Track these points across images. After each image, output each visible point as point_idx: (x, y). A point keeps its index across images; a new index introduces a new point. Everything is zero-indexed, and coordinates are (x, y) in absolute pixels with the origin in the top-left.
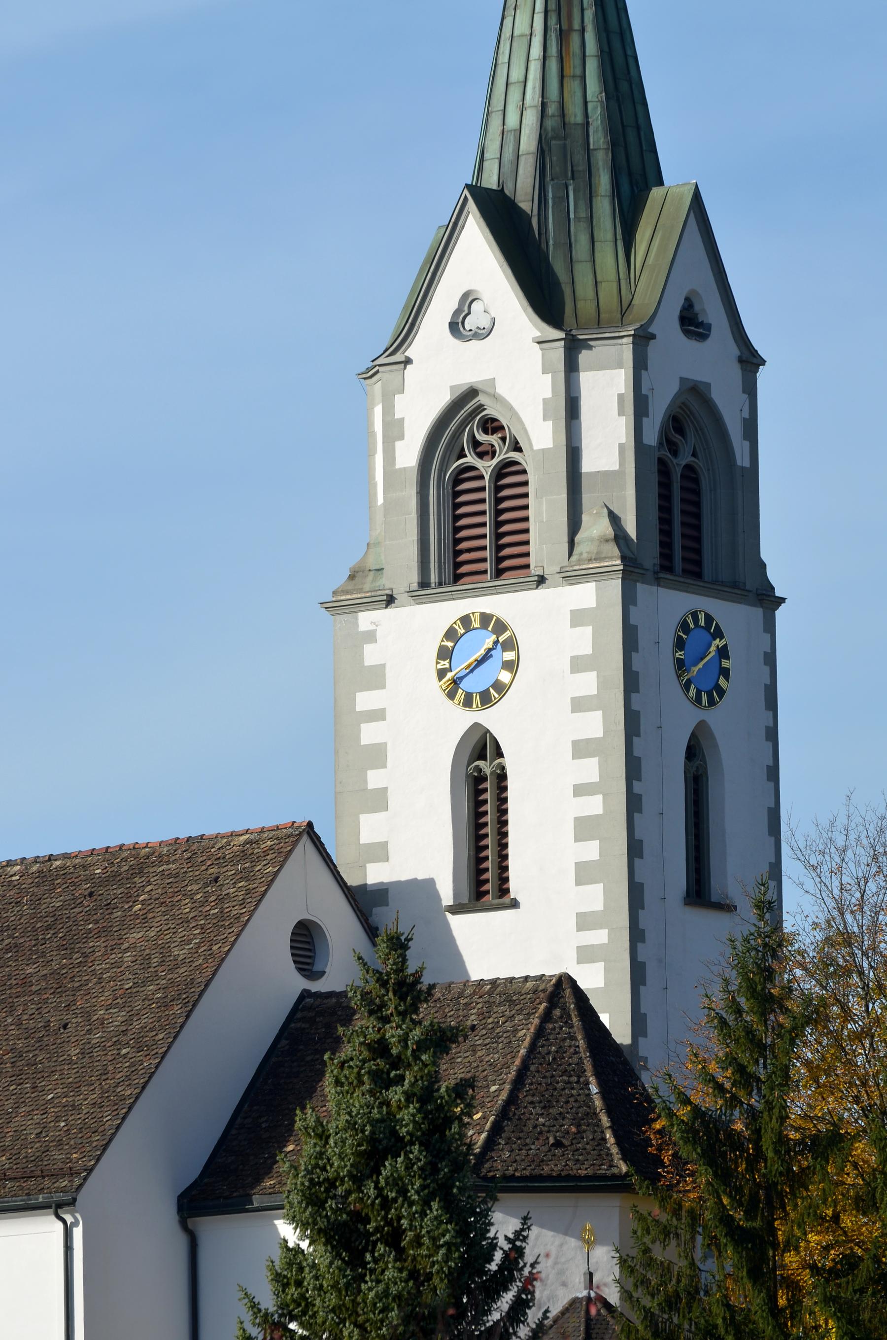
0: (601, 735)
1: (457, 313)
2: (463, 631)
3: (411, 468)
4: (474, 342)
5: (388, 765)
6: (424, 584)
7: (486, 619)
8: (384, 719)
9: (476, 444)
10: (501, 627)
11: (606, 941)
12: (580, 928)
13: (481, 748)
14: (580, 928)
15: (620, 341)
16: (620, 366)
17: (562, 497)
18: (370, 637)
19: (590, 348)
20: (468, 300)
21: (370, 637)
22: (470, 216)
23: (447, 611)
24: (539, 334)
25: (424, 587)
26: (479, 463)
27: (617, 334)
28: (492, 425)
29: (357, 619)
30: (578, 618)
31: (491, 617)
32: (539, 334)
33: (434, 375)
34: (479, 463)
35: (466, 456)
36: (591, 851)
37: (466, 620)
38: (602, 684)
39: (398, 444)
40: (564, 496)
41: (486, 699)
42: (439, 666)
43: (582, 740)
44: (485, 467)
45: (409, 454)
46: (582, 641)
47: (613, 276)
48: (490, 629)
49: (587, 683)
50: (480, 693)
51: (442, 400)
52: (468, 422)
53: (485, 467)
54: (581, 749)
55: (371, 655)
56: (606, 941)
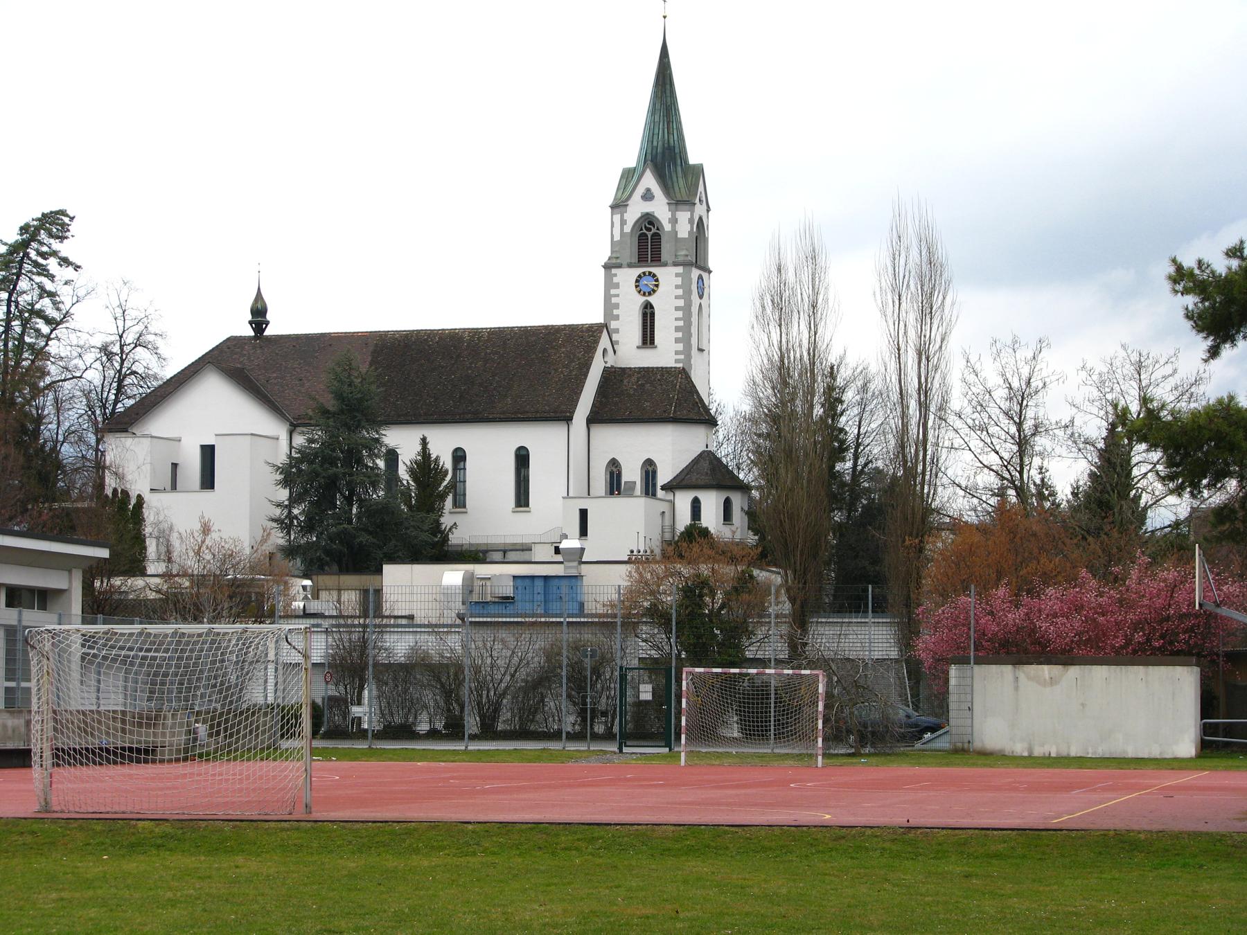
10: (654, 276)
23: (640, 271)
30: (677, 275)
36: (680, 335)
41: (650, 294)
44: (649, 234)
52: (648, 221)
53: (649, 234)
54: (677, 309)
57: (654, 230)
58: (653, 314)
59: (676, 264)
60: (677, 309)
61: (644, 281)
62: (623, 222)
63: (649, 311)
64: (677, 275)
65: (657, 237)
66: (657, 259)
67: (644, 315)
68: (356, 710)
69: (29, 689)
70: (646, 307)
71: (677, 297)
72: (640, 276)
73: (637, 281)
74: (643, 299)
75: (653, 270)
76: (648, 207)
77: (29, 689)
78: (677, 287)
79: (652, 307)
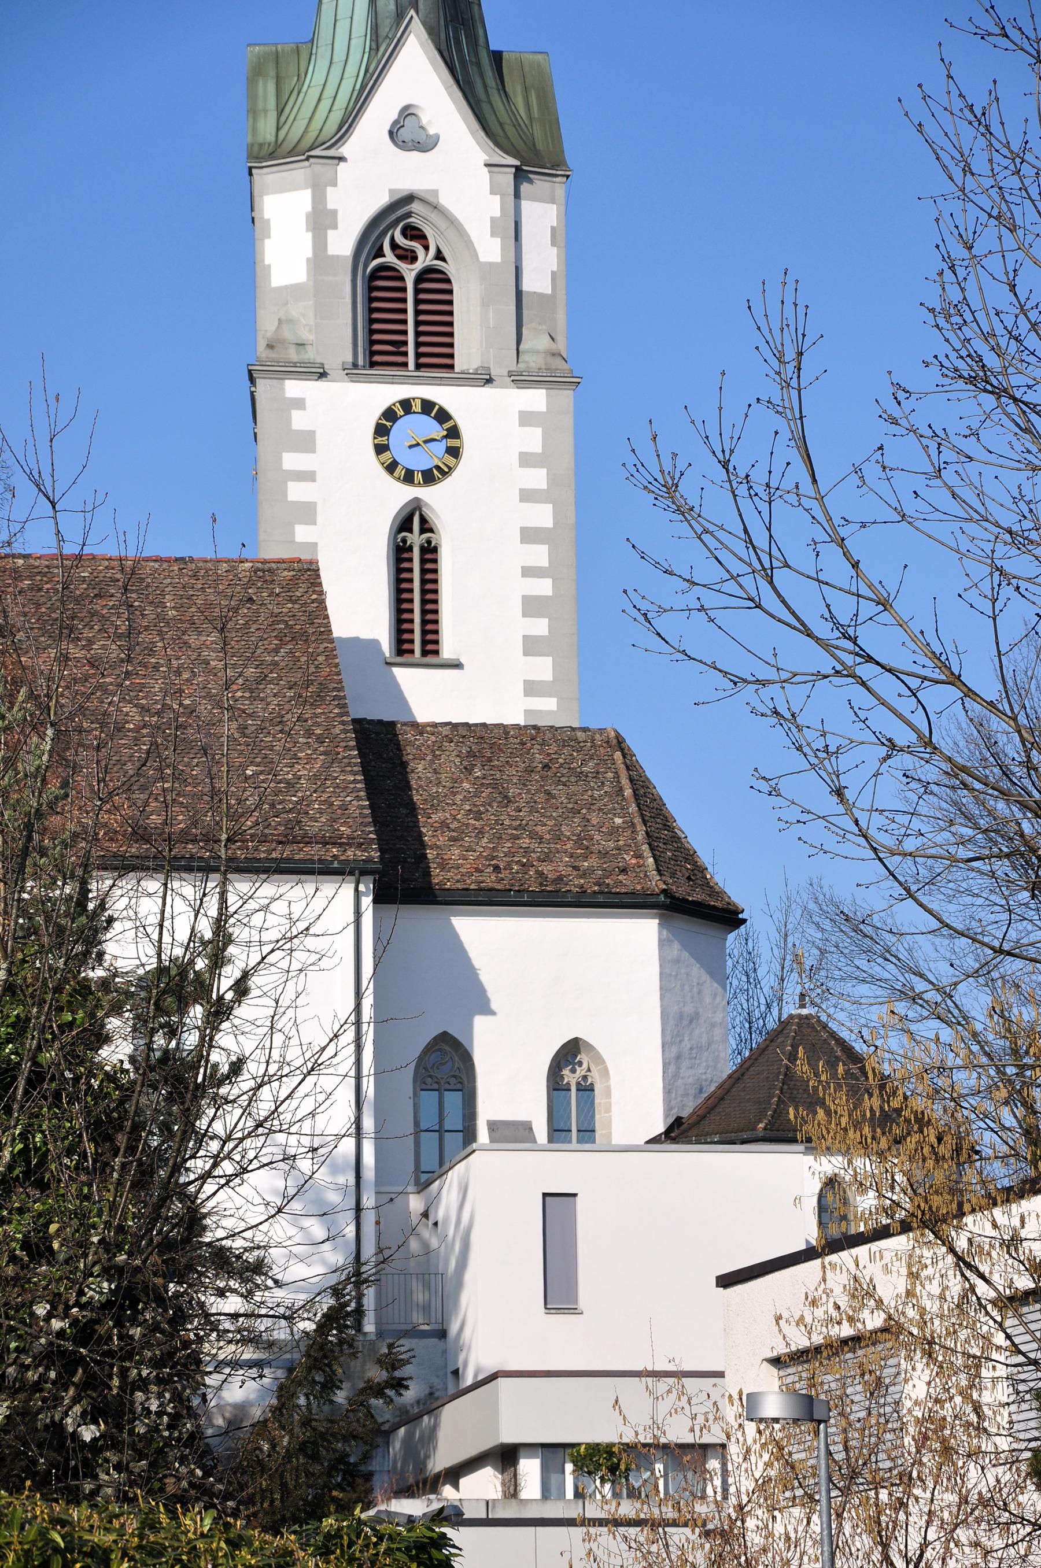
0: (551, 526)
1: (396, 122)
2: (402, 413)
3: (345, 257)
4: (415, 154)
5: (320, 519)
6: (355, 365)
7: (427, 406)
8: (314, 481)
9: (394, 246)
10: (443, 416)
11: (555, 708)
12: (527, 693)
13: (412, 520)
14: (527, 693)
15: (554, 179)
16: (552, 201)
17: (513, 308)
18: (299, 403)
19: (531, 181)
20: (407, 112)
21: (299, 403)
22: (412, 35)
23: (387, 393)
24: (487, 158)
25: (352, 371)
26: (402, 266)
27: (554, 172)
28: (414, 233)
29: (283, 384)
30: (526, 418)
31: (434, 404)
32: (487, 158)
33: (368, 176)
34: (402, 266)
35: (384, 256)
36: (540, 627)
37: (406, 405)
38: (552, 479)
39: (330, 233)
40: (514, 308)
42: (376, 442)
43: (532, 528)
44: (410, 273)
45: (343, 242)
46: (533, 440)
47: (509, 121)
48: (437, 407)
49: (538, 478)
50: (422, 472)
51: (383, 200)
52: (399, 224)
53: (410, 273)
54: (529, 535)
55: (299, 420)
56: (555, 708)
57: (424, 260)
58: (430, 551)
59: (520, 380)
60: (529, 535)
61: (410, 428)
62: (321, 220)
63: (415, 539)
64: (526, 418)
65: (435, 283)
66: (437, 356)
67: (400, 553)
68: (973, 1472)
69: (570, 1142)
70: (404, 524)
71: (527, 496)
72: (390, 414)
73: (381, 430)
74: (407, 493)
75: (442, 395)
76: (410, 173)
77: (570, 1142)
78: (526, 460)
79: (426, 527)
